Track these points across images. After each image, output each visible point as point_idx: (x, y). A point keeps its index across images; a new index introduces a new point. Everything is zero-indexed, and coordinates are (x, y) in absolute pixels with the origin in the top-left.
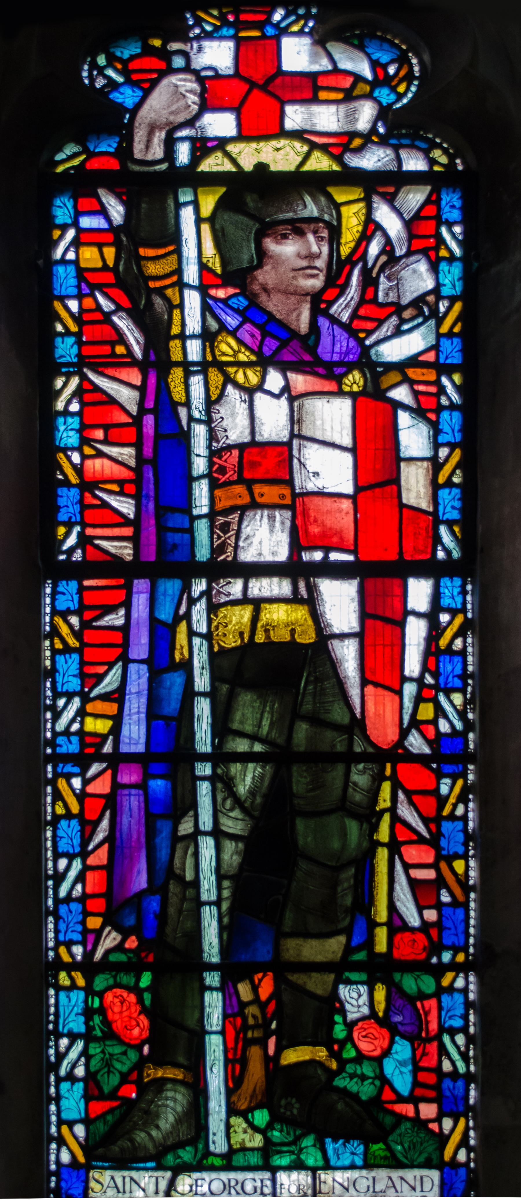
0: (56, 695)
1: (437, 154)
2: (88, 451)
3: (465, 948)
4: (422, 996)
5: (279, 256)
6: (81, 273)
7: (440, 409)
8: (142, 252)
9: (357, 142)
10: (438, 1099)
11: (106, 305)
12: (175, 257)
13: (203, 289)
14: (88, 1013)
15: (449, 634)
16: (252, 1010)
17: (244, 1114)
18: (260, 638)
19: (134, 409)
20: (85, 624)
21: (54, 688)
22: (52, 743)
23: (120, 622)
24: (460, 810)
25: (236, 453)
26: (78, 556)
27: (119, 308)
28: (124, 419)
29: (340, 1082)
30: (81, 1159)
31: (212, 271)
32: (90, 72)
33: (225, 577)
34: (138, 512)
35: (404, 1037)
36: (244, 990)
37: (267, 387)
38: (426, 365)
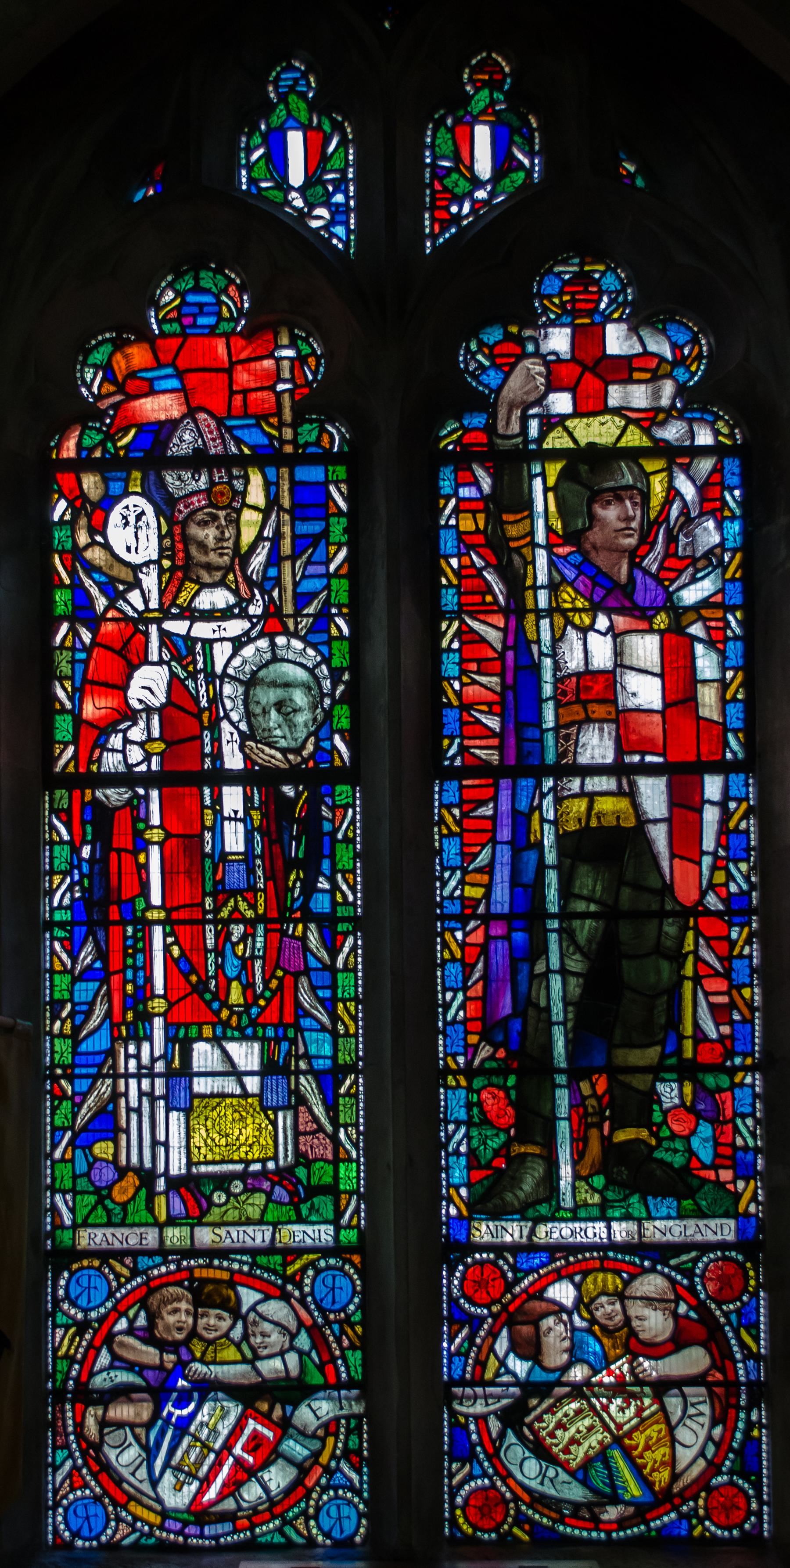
0: (444, 869)
1: (720, 424)
2: (465, 679)
3: (752, 1054)
4: (720, 1090)
5: (605, 519)
6: (461, 536)
7: (727, 639)
8: (505, 517)
9: (661, 416)
10: (733, 1167)
11: (478, 562)
12: (528, 521)
13: (549, 547)
14: (469, 1106)
15: (736, 817)
16: (592, 1102)
17: (586, 1179)
18: (594, 823)
19: (499, 646)
20: (464, 815)
21: (441, 864)
22: (441, 906)
23: (490, 812)
24: (746, 951)
25: (574, 679)
26: (458, 762)
27: (488, 565)
28: (491, 654)
29: (658, 1155)
30: (465, 1213)
31: (555, 532)
32: (465, 356)
33: (567, 776)
34: (502, 727)
35: (706, 1120)
36: (585, 1087)
37: (596, 627)
38: (715, 606)
